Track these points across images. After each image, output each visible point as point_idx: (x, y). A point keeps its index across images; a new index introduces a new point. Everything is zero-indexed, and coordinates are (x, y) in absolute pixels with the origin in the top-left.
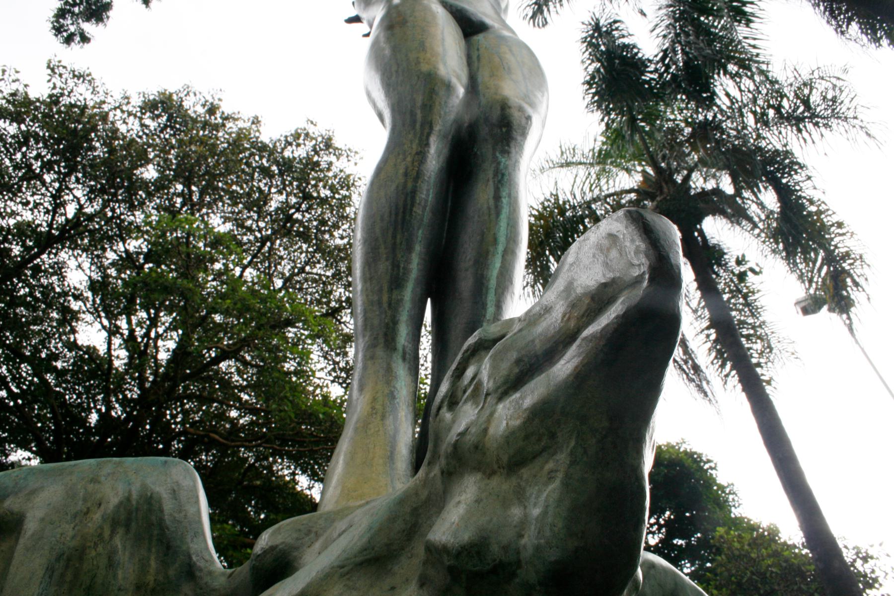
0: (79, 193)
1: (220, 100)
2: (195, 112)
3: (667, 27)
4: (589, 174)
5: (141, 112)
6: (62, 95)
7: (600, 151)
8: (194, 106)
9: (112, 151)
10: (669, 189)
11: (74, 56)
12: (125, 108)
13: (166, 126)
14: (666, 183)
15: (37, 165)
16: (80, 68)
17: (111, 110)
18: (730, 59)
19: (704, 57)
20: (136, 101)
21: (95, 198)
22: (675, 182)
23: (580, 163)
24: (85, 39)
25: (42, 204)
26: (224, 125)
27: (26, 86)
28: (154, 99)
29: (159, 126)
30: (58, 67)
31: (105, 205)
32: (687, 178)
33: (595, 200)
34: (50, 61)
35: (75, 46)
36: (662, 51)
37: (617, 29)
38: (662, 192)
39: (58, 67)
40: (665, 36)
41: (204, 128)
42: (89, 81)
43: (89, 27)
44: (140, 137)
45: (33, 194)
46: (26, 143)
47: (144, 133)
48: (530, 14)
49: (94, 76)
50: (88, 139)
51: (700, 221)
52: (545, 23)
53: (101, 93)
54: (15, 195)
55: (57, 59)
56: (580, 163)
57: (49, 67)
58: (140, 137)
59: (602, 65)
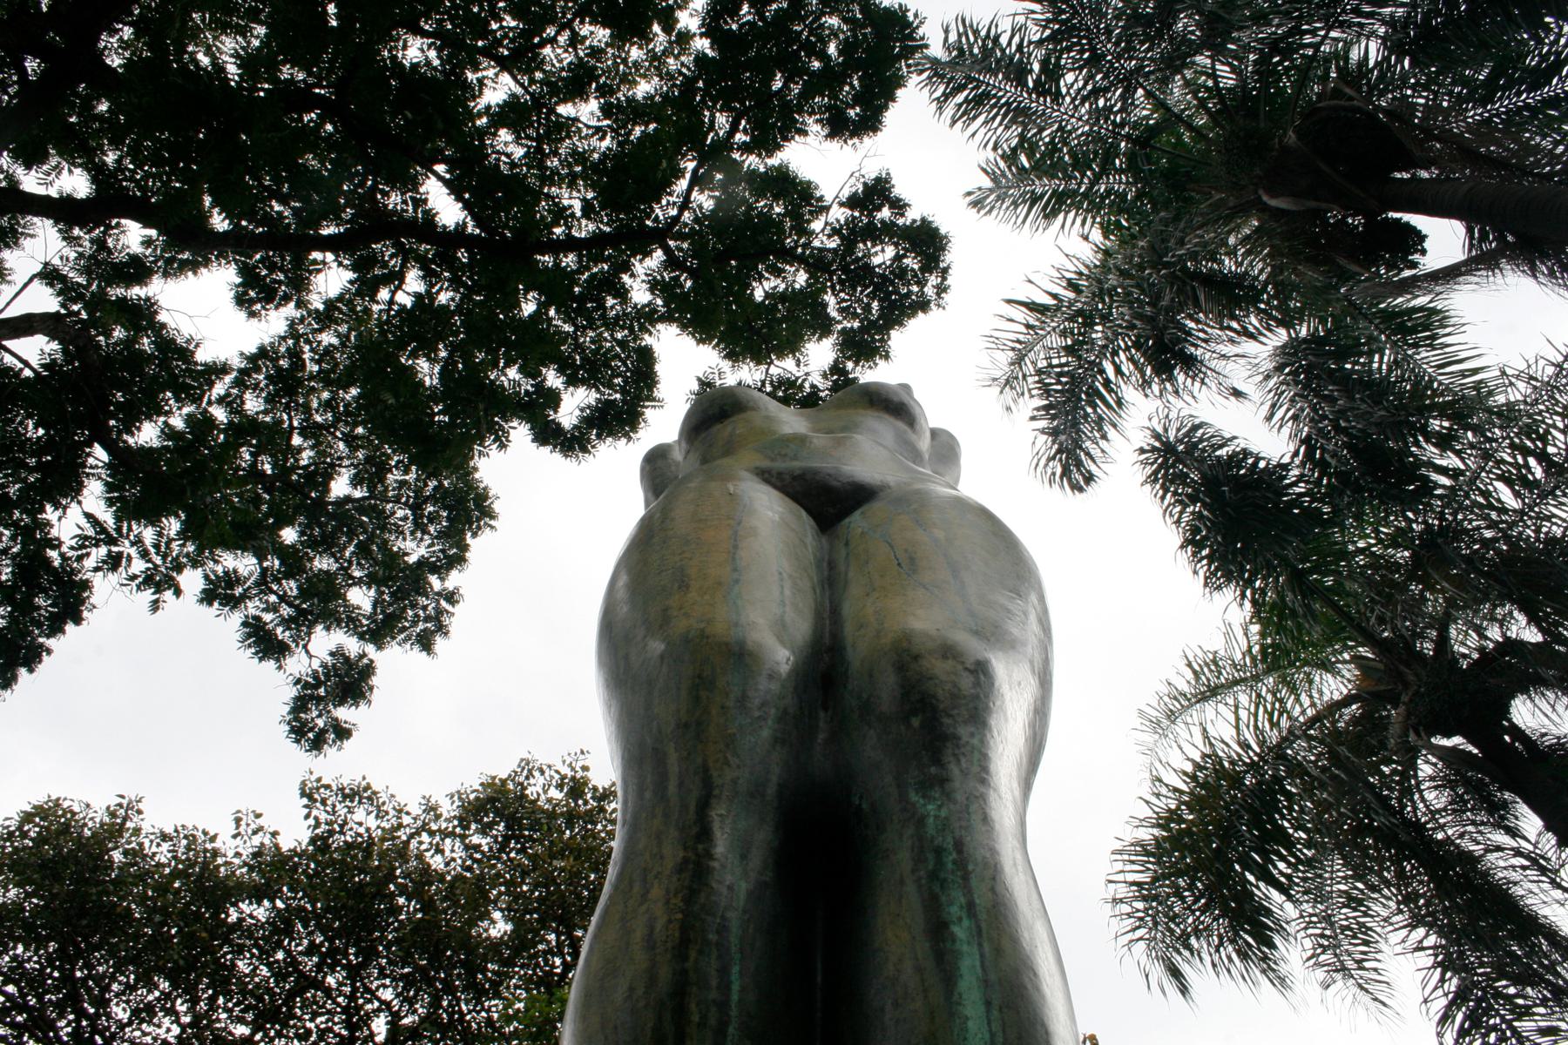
0: (387, 995)
1: (585, 768)
2: (549, 800)
3: (1292, 401)
4: (1259, 696)
5: (460, 825)
6: (331, 833)
7: (1263, 649)
8: (545, 792)
9: (428, 906)
10: (1416, 675)
11: (336, 766)
12: (434, 827)
13: (507, 839)
14: (1408, 666)
15: (309, 963)
16: (350, 778)
17: (412, 836)
18: (1425, 411)
19: (1377, 425)
20: (448, 809)
21: (416, 995)
22: (1421, 656)
23: (1236, 682)
24: (343, 733)
25: (330, 1030)
26: (602, 810)
27: (275, 834)
28: (477, 798)
29: (496, 841)
30: (318, 789)
31: (435, 1003)
32: (1443, 642)
33: (1287, 740)
34: (304, 783)
35: (330, 751)
36: (1302, 442)
37: (1201, 440)
38: (1406, 685)
39: (318, 789)
40: (1295, 418)
41: (570, 825)
42: (369, 798)
43: (343, 713)
44: (469, 869)
45: (315, 1015)
46: (289, 931)
47: (475, 860)
48: (1059, 470)
49: (375, 787)
50: (386, 896)
51: (1505, 711)
52: (1089, 478)
53: (392, 812)
54: (285, 1025)
55: (313, 778)
56: (1236, 682)
57: (303, 794)
58: (469, 869)
59: (1204, 505)
